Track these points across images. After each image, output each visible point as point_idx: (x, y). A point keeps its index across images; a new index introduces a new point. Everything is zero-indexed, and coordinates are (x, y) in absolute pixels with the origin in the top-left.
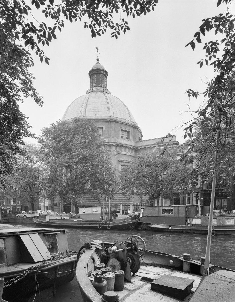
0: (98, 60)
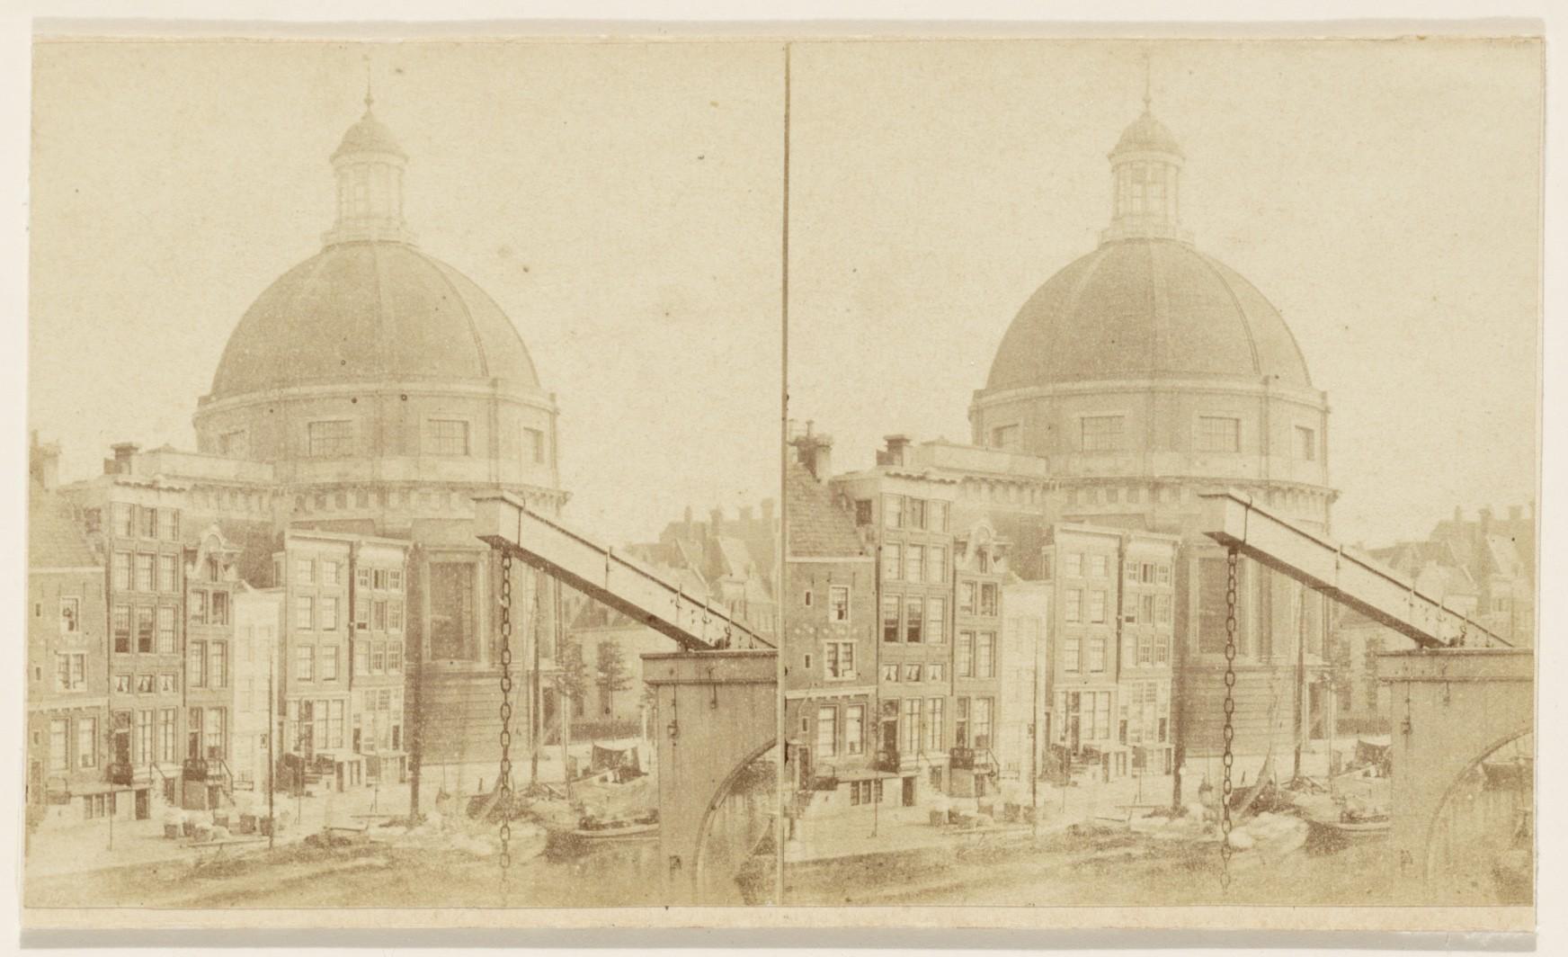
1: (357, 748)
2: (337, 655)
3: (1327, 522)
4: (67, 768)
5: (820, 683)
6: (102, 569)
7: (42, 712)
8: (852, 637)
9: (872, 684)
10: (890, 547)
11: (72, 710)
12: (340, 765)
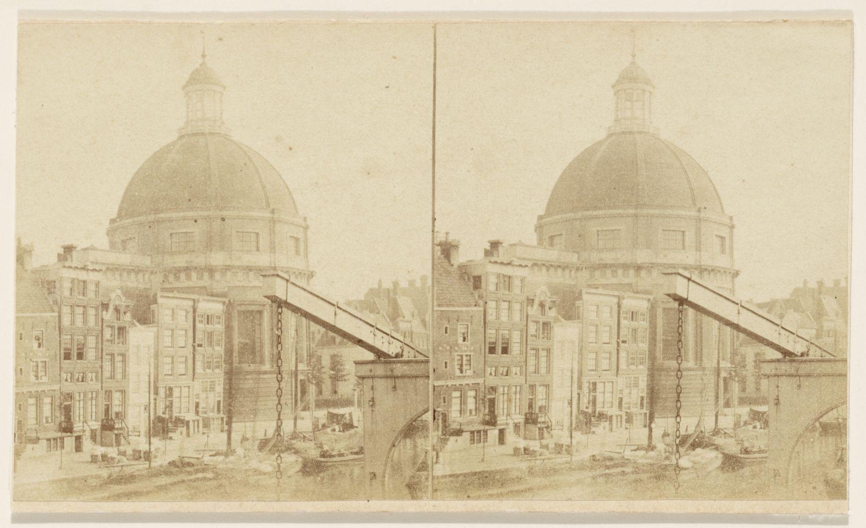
0: (204, 56)
1: (197, 413)
2: (186, 361)
3: (733, 288)
4: (37, 424)
5: (453, 377)
6: (56, 314)
7: (23, 393)
8: (471, 351)
9: (482, 377)
10: (492, 302)
11: (40, 391)
12: (188, 422)
